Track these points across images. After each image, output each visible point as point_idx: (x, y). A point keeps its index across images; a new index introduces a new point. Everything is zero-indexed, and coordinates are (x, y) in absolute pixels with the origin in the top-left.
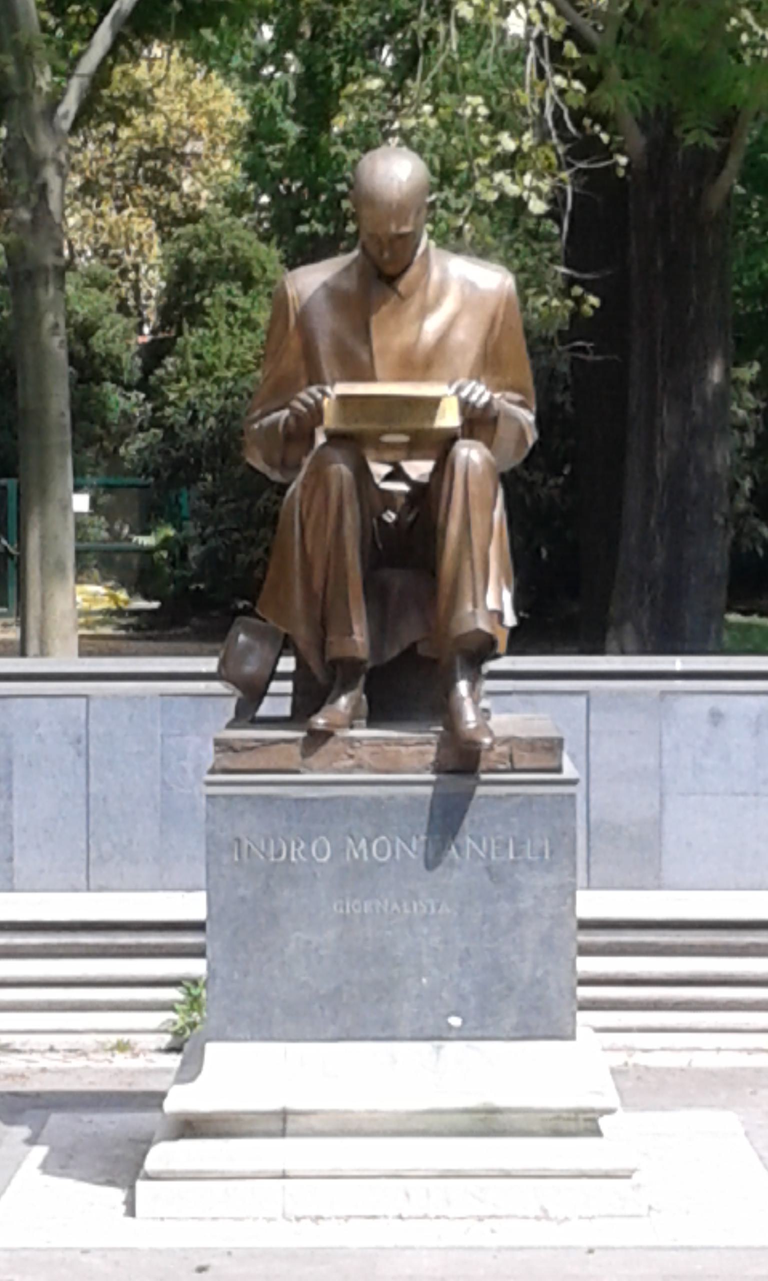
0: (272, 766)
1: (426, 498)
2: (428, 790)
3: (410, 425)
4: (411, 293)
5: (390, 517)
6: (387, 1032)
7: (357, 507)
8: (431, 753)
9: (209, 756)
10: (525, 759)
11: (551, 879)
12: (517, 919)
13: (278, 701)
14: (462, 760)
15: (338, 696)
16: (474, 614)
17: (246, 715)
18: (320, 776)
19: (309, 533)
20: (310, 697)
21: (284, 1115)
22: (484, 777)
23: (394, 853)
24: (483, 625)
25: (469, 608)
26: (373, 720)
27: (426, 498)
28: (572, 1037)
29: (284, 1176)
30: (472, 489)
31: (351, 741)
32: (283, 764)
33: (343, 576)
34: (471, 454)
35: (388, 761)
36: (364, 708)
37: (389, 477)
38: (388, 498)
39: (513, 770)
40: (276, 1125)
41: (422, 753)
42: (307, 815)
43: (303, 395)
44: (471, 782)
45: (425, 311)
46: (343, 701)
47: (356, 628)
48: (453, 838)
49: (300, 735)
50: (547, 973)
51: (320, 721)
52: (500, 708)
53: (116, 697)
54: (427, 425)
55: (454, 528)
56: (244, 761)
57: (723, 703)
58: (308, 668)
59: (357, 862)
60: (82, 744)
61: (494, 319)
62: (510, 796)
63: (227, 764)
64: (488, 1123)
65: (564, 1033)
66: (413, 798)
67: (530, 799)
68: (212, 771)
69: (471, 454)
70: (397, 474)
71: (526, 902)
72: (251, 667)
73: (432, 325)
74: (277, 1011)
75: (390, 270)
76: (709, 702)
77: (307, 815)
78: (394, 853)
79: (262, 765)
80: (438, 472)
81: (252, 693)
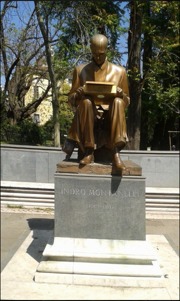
0: (71, 171)
1: (108, 114)
2: (110, 179)
3: (104, 92)
4: (104, 69)
5: (99, 118)
6: (99, 236)
7: (92, 111)
8: (110, 170)
9: (56, 169)
10: (132, 172)
11: (139, 202)
12: (131, 210)
13: (75, 155)
14: (117, 173)
15: (87, 156)
16: (120, 137)
17: (68, 159)
18: (83, 175)
19: (80, 118)
20: (81, 156)
21: (74, 257)
22: (123, 176)
23: (101, 194)
24: (123, 140)
25: (119, 136)
26: (95, 162)
27: (108, 114)
28: (145, 240)
29: (73, 273)
30: (119, 108)
31: (90, 166)
32: (74, 171)
33: (89, 128)
34: (118, 101)
35: (101, 172)
36: (93, 159)
37: (99, 109)
38: (99, 114)
39: (130, 175)
40: (72, 259)
41: (108, 170)
42: (78, 183)
43: (79, 88)
44: (120, 178)
45: (106, 74)
46: (88, 157)
47: (92, 140)
48: (116, 191)
49: (78, 164)
50: (138, 224)
51: (83, 162)
52: (123, 158)
53: (53, 153)
54: (109, 93)
55: (115, 117)
56: (64, 170)
57: (150, 158)
58: (81, 149)
59: (92, 195)
60: (47, 160)
61: (121, 77)
62: (129, 181)
63: (60, 170)
64: (125, 261)
65: (143, 238)
66: (105, 181)
67: (134, 182)
68: (56, 172)
69: (118, 101)
70: (101, 108)
71: (133, 207)
72: (69, 148)
73: (108, 77)
74: (72, 230)
75: (99, 63)
76: (147, 158)
77: (78, 183)
78: (101, 194)
79: (69, 171)
80: (110, 107)
81: (69, 153)
